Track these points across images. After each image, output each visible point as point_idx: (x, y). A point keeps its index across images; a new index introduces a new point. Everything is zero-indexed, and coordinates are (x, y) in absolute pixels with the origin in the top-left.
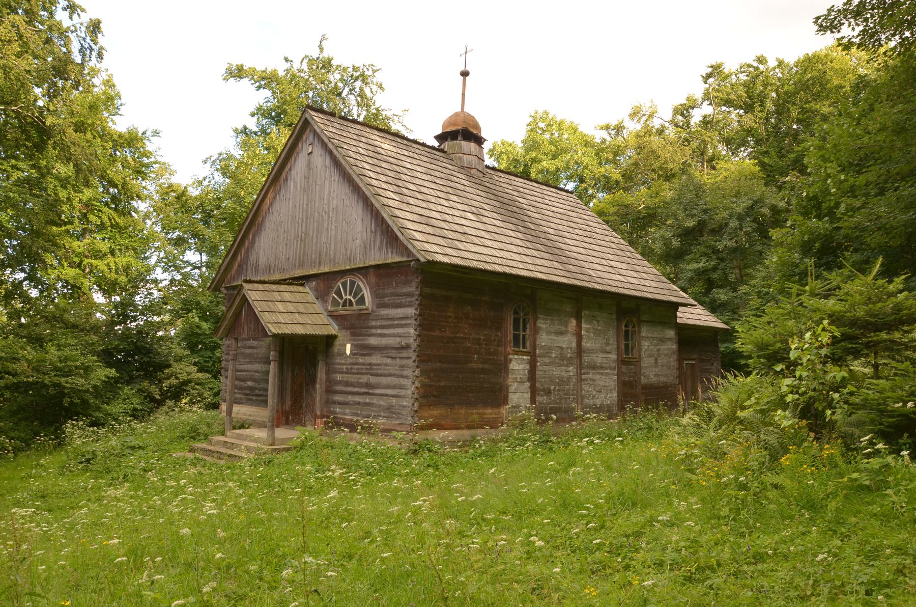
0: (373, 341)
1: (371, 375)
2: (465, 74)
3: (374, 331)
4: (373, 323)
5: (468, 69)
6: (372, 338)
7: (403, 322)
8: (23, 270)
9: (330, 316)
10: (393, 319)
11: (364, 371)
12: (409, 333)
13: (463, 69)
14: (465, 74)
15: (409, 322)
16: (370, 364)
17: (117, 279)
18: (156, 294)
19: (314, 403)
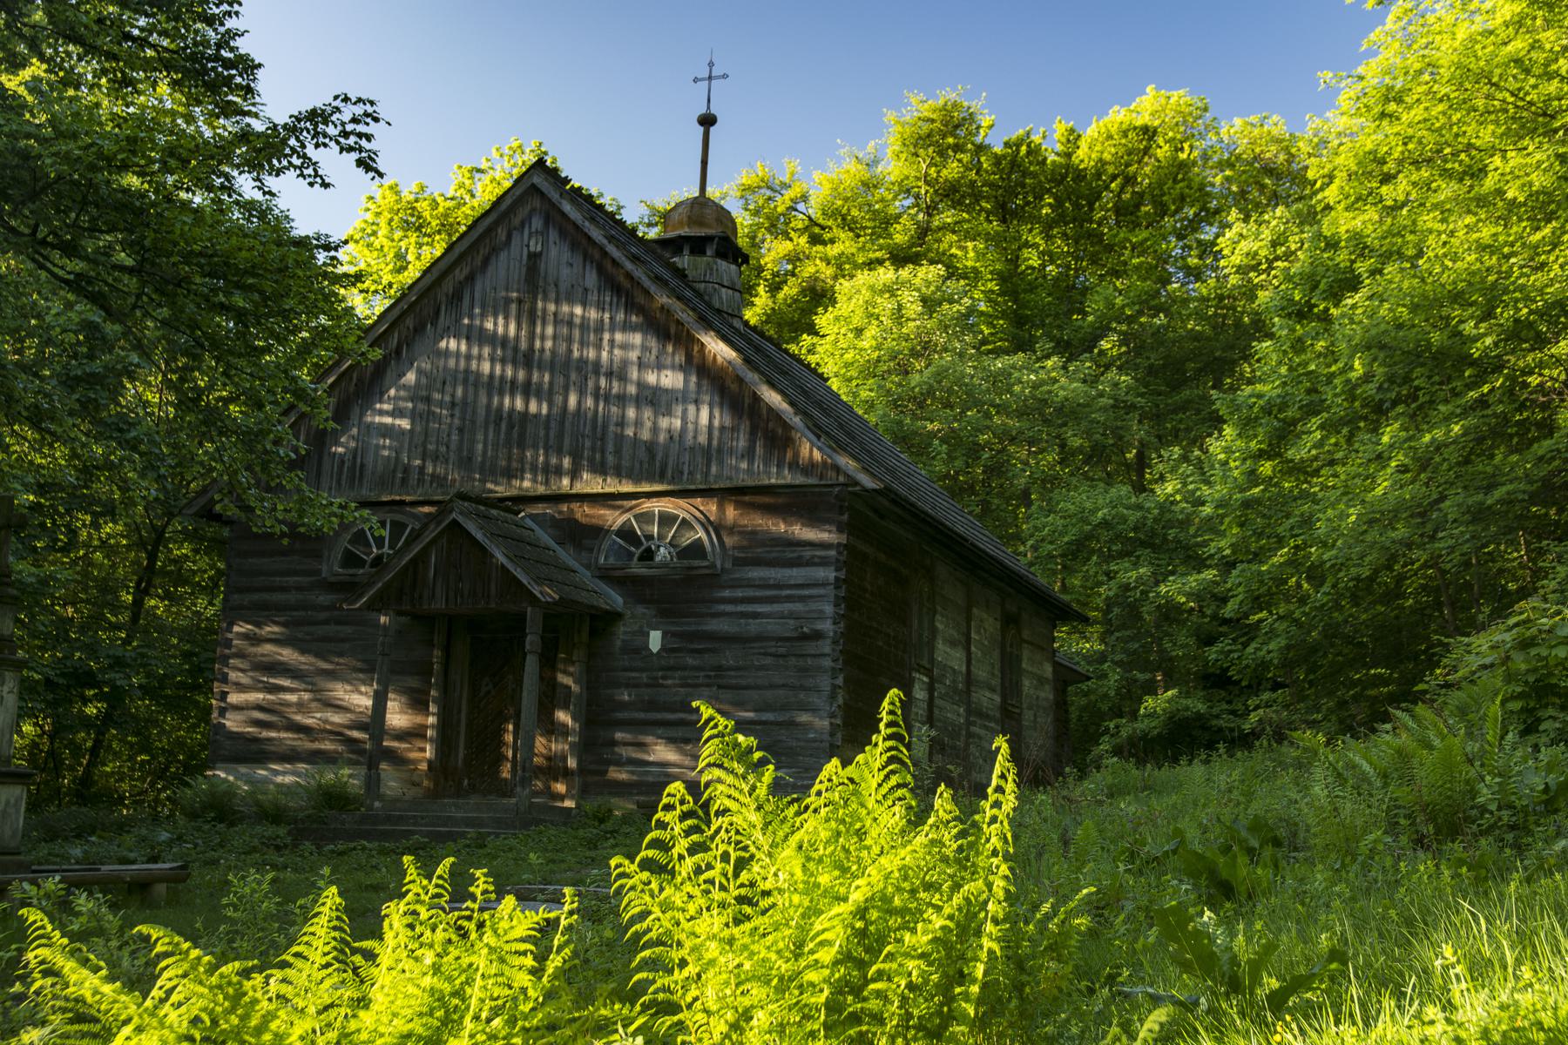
0: (714, 625)
1: (719, 687)
2: (707, 121)
3: (722, 607)
4: (727, 593)
5: (713, 111)
6: (715, 621)
7: (806, 592)
8: (1166, 270)
9: (600, 578)
10: (778, 586)
11: (701, 681)
12: (821, 611)
13: (703, 111)
14: (707, 121)
15: (822, 591)
16: (719, 668)
17: (846, 763)
18: (1459, 969)
19: (519, 682)
